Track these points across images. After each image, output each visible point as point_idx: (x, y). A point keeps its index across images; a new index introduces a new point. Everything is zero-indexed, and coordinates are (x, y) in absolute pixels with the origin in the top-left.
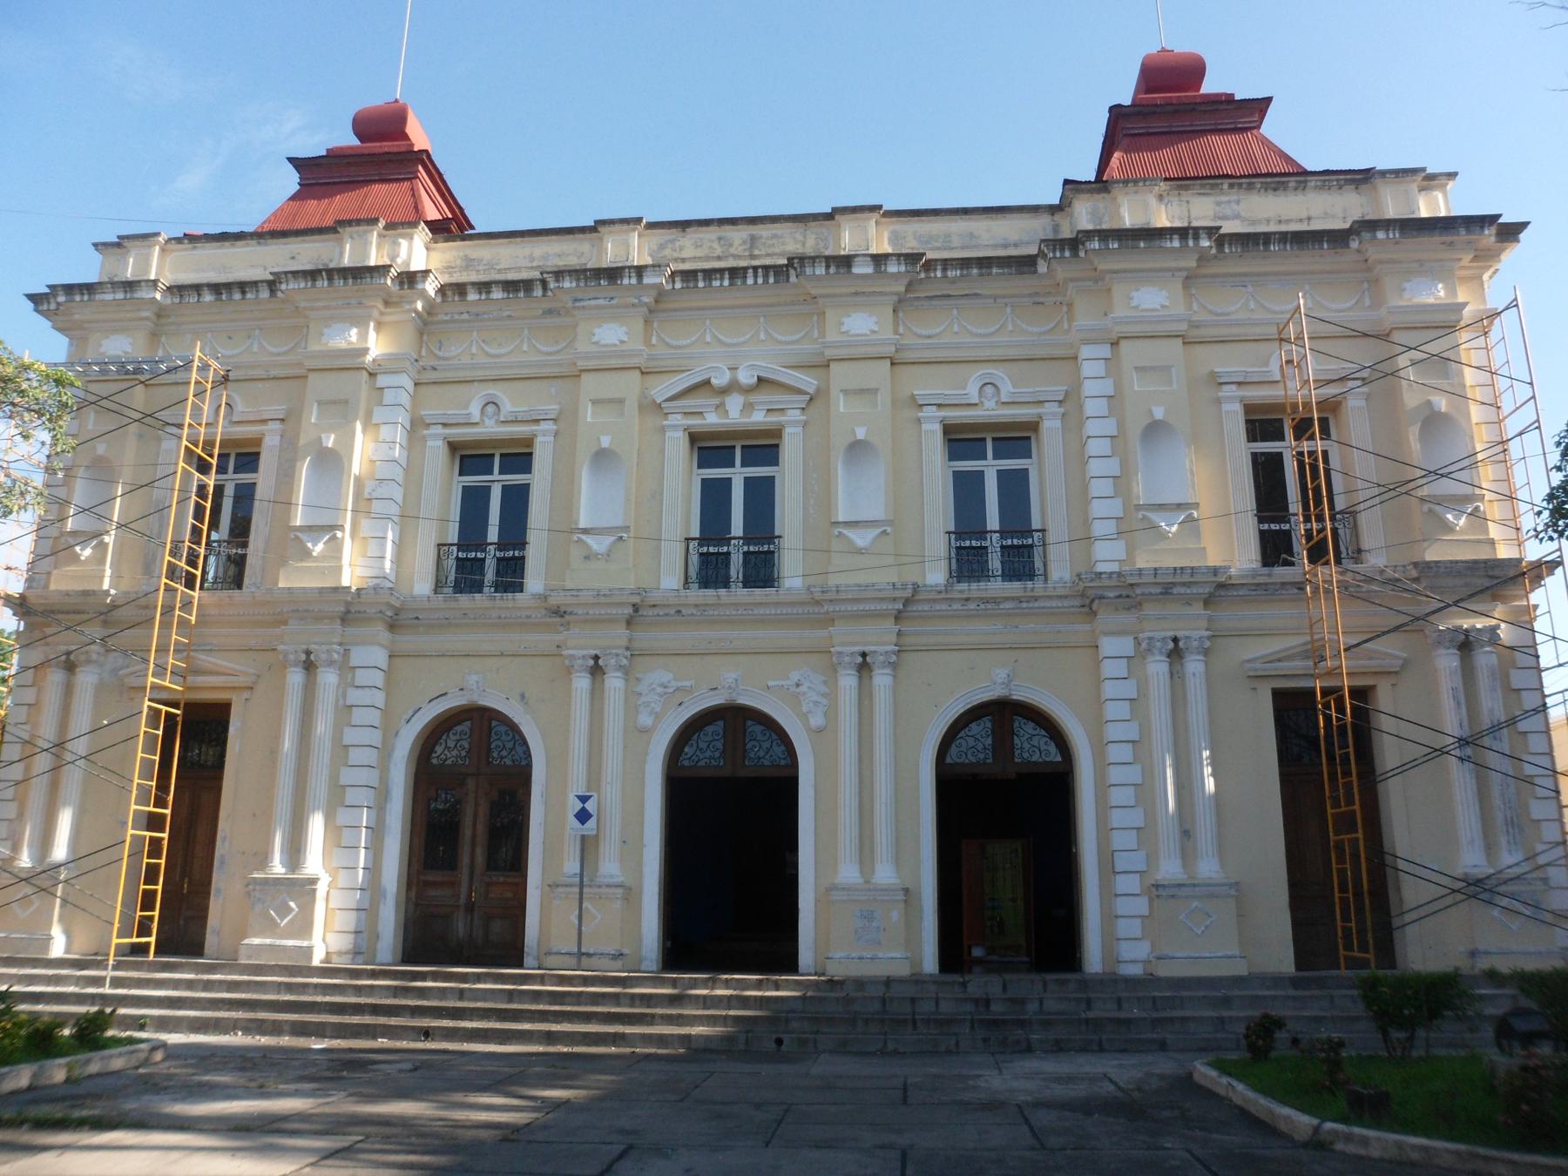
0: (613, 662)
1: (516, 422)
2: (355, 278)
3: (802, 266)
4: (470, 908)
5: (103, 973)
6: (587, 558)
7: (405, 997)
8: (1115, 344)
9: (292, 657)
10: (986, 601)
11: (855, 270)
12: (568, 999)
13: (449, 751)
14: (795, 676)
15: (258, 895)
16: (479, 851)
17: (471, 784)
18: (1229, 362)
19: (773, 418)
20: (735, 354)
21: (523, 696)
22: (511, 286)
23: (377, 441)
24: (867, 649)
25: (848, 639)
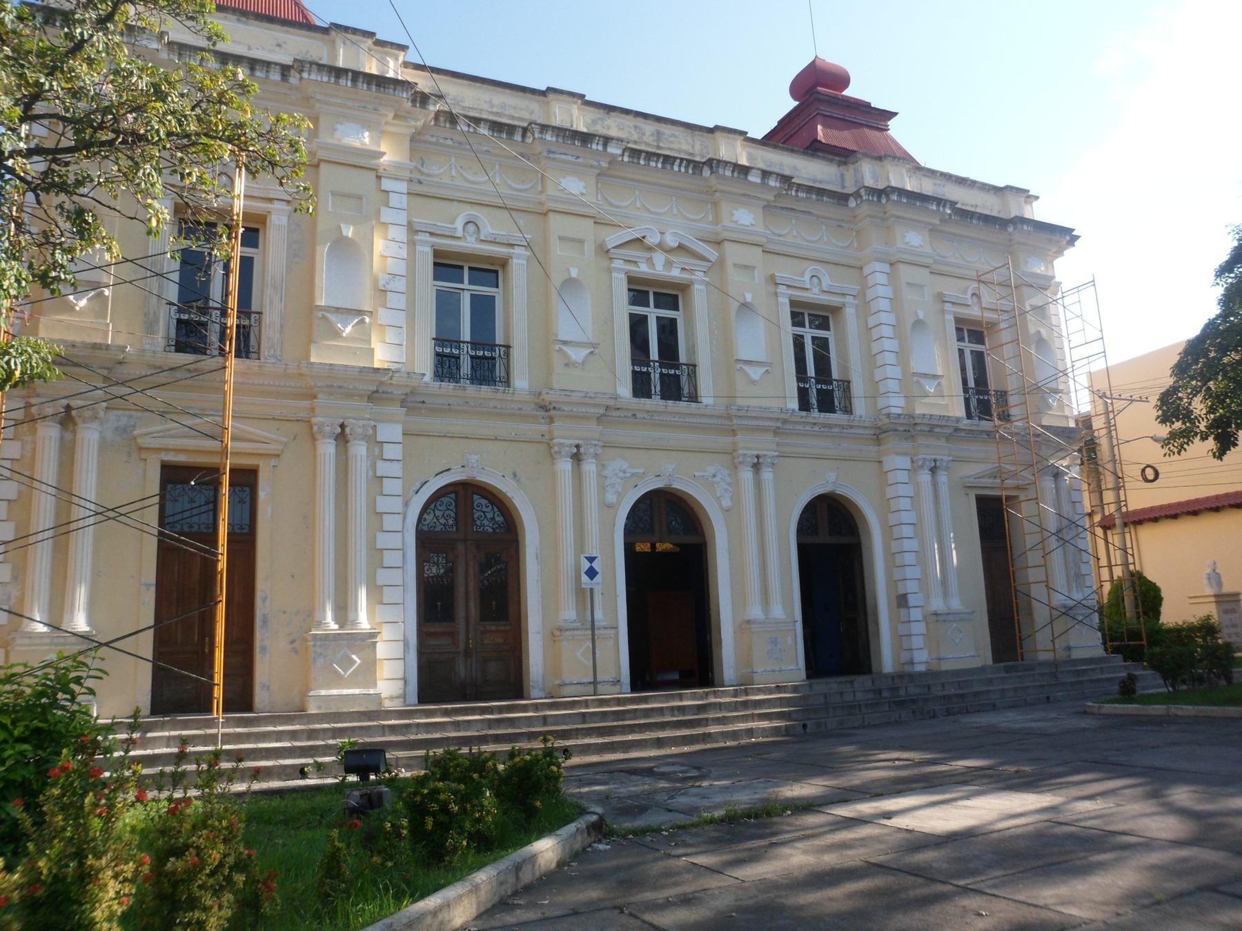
0: (592, 450)
1: (493, 242)
2: (378, 85)
3: (718, 167)
4: (467, 653)
5: (214, 731)
6: (567, 365)
7: (499, 728)
8: (891, 264)
9: (328, 429)
10: (825, 425)
11: (751, 178)
12: (627, 716)
13: (443, 519)
14: (711, 470)
15: (319, 650)
16: (472, 605)
17: (461, 548)
18: (950, 288)
19: (686, 276)
20: (663, 224)
21: (515, 475)
22: (496, 127)
23: (386, 239)
24: (761, 453)
25: (749, 445)
